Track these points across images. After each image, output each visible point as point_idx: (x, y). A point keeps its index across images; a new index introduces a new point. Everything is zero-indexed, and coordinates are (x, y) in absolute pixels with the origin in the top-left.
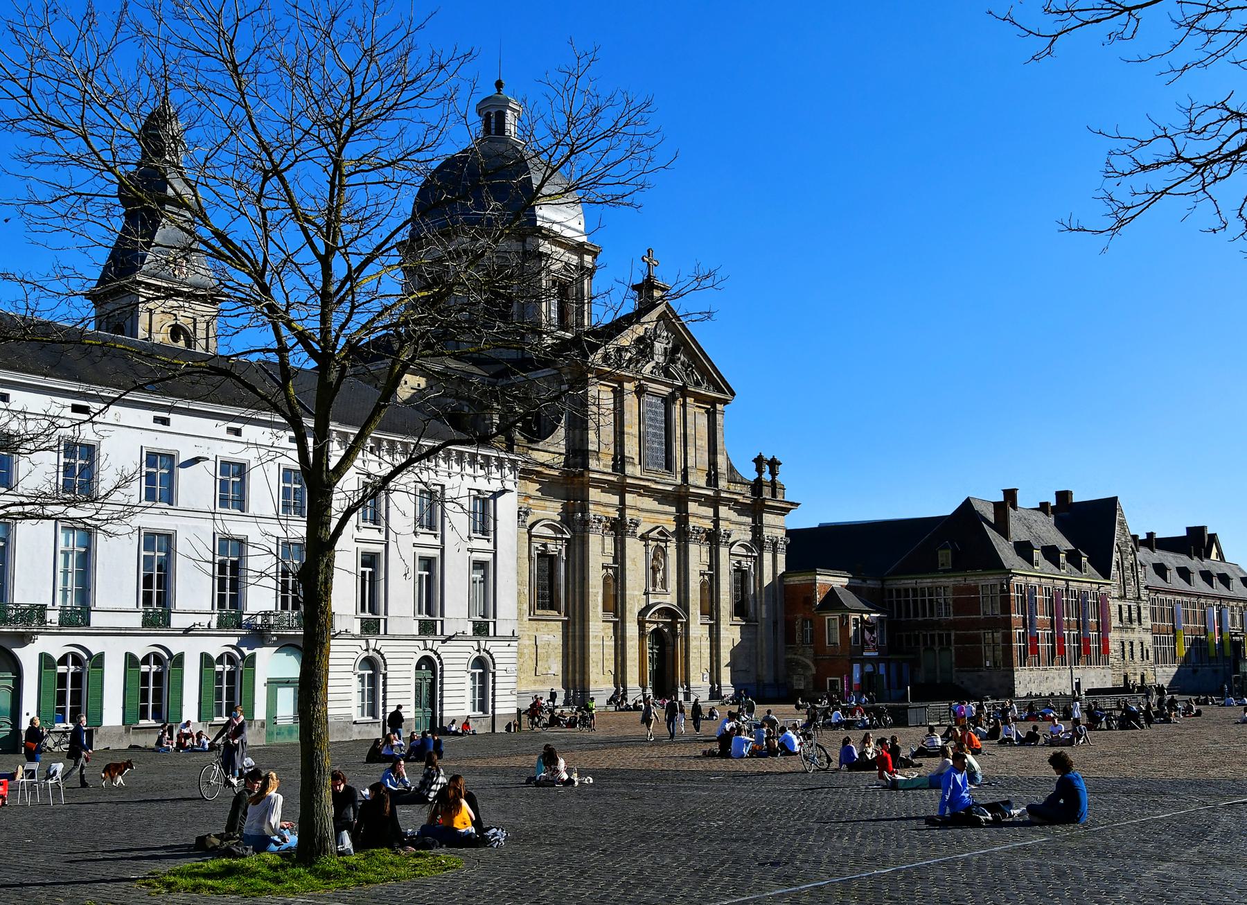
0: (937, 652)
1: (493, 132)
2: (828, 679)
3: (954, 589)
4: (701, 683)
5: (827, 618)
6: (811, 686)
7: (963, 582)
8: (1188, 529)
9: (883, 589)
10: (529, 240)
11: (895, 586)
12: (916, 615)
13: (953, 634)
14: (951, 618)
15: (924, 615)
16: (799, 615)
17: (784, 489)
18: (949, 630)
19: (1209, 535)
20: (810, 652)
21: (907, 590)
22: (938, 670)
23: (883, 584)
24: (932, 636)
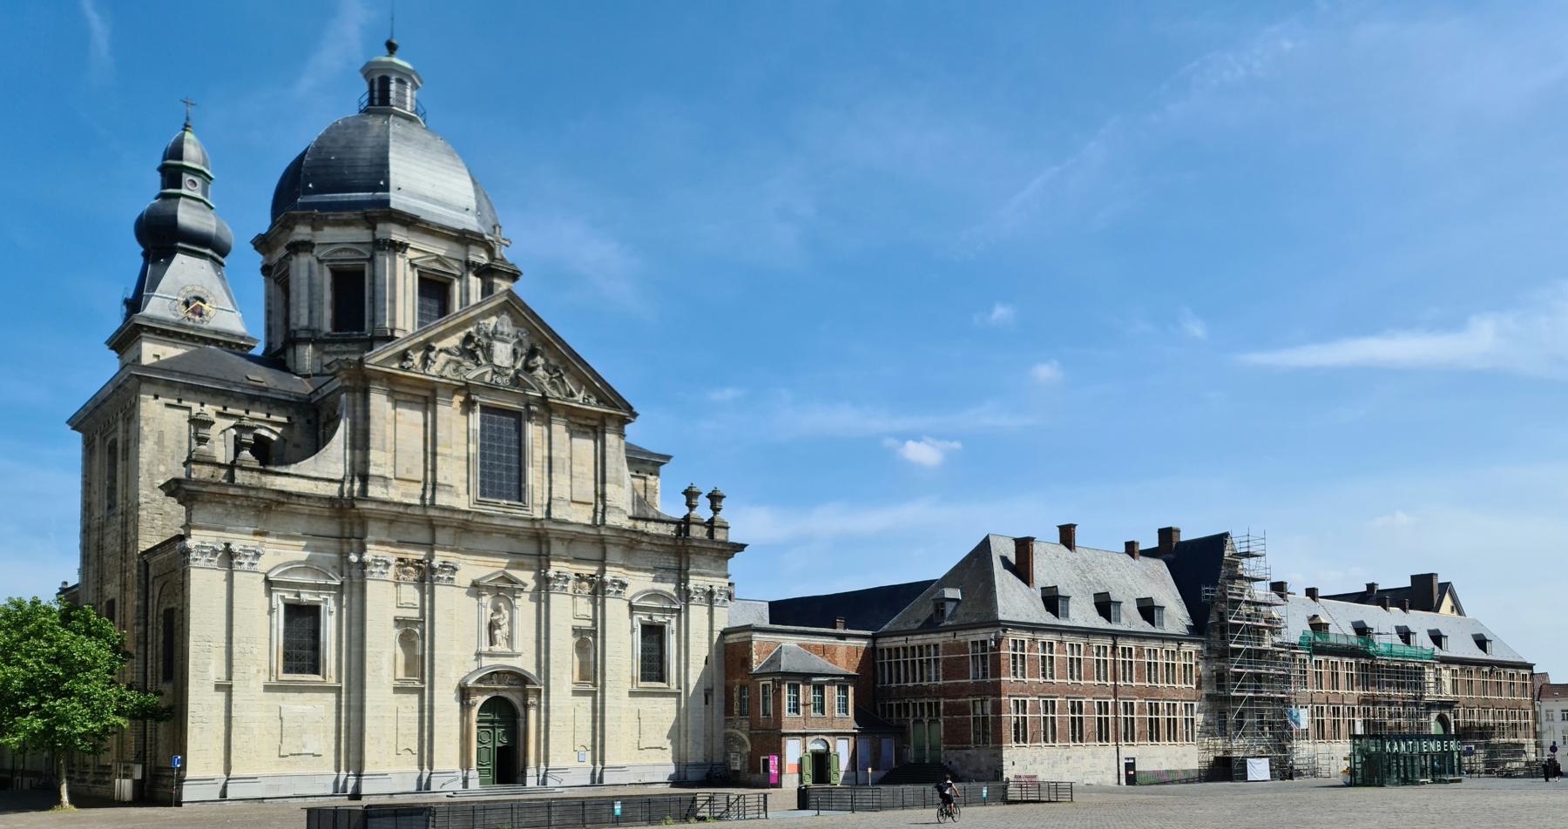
0: (926, 724)
1: (376, 102)
2: (762, 758)
3: (944, 647)
4: (572, 763)
5: (761, 683)
6: (746, 766)
7: (952, 638)
8: (1414, 578)
10: (380, 227)
11: (886, 645)
12: (906, 680)
13: (942, 703)
14: (941, 682)
15: (914, 680)
16: (738, 680)
17: (727, 528)
18: (938, 698)
19: (1440, 584)
20: (746, 724)
21: (897, 649)
22: (927, 748)
23: (874, 643)
24: (922, 705)
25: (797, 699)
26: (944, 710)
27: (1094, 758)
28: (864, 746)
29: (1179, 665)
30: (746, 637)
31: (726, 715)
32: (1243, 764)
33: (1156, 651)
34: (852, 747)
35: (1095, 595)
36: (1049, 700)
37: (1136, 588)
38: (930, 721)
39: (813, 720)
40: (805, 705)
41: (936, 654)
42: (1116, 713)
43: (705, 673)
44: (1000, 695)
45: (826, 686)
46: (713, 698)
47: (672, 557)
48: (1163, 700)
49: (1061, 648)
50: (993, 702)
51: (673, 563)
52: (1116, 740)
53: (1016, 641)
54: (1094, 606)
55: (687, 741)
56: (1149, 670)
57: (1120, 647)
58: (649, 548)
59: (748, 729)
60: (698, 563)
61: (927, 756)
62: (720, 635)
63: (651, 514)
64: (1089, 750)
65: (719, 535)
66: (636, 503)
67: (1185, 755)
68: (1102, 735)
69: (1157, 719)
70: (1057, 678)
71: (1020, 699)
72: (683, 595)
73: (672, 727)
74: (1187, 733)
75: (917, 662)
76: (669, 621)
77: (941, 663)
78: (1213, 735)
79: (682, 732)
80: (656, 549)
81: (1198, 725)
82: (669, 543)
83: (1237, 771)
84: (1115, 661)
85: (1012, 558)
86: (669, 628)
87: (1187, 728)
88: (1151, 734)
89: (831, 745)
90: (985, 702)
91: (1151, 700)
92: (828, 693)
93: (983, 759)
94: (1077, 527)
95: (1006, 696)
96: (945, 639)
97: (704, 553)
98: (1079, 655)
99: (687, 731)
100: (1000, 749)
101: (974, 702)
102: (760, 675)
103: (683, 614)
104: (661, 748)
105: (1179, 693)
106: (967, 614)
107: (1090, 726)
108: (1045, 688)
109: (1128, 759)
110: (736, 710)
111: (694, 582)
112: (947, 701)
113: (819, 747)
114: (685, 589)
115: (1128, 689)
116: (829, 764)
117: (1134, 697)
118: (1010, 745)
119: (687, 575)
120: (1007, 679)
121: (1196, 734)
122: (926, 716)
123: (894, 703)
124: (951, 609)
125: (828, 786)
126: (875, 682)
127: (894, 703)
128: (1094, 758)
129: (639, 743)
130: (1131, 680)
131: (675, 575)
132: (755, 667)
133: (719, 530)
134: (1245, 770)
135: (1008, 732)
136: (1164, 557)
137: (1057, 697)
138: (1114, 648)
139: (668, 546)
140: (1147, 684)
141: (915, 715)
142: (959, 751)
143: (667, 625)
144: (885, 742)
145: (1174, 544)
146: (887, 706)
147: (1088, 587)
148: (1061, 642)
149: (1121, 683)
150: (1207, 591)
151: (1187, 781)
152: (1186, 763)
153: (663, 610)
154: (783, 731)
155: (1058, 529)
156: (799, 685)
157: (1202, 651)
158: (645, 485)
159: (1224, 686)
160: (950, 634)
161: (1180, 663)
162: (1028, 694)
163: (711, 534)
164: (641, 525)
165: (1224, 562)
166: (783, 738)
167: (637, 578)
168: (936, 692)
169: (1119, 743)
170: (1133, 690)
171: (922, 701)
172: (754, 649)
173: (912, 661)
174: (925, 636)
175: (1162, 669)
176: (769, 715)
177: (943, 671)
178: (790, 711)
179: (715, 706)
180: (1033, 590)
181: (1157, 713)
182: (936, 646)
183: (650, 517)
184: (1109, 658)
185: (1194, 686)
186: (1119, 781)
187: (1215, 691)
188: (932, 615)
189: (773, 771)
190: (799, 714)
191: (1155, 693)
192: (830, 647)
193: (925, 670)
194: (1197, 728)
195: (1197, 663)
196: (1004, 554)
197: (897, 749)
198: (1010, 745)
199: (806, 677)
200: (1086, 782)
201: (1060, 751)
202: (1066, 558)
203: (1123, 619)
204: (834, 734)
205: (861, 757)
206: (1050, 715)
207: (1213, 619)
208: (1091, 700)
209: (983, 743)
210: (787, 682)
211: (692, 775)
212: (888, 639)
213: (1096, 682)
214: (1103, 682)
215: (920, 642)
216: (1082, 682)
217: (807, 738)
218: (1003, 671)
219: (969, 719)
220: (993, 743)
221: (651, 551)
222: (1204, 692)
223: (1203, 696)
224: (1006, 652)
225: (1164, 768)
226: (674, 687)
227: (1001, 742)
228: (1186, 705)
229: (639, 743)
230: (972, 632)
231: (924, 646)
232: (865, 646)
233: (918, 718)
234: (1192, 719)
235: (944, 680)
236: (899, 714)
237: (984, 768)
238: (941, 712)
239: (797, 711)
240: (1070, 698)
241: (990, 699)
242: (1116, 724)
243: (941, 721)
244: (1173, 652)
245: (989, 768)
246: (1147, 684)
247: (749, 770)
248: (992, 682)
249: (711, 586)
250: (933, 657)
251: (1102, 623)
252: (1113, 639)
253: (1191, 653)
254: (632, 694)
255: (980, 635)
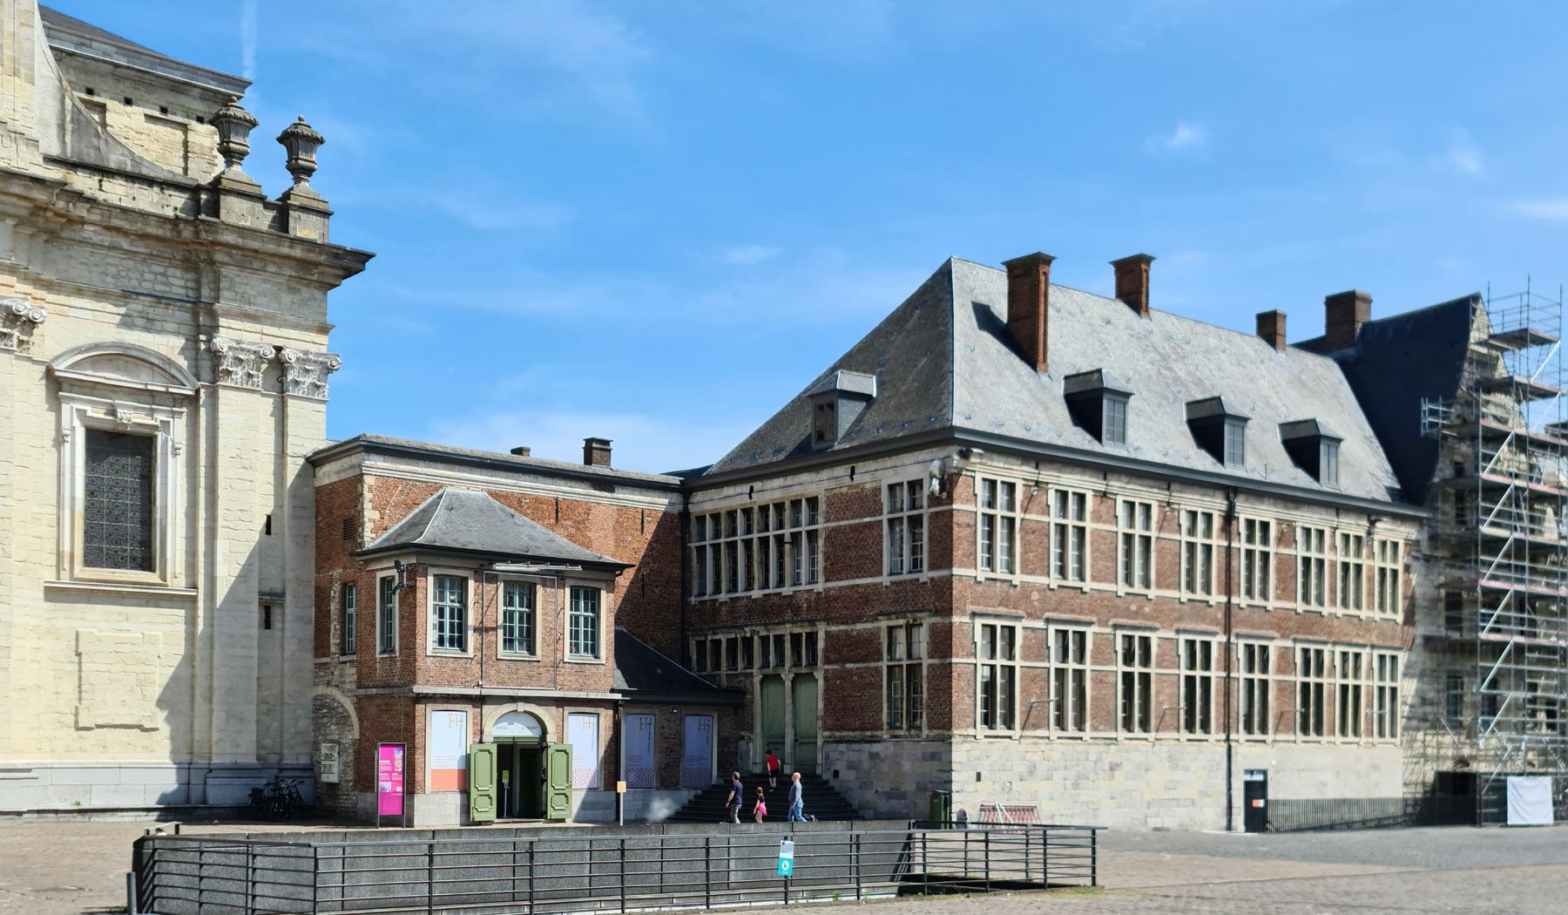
0: (788, 684)
3: (830, 503)
6: (351, 776)
7: (847, 480)
9: (685, 515)
12: (749, 587)
13: (821, 635)
14: (820, 587)
15: (766, 585)
16: (337, 573)
18: (812, 622)
20: (351, 671)
21: (732, 514)
22: (789, 740)
23: (686, 503)
24: (779, 639)
25: (461, 613)
26: (826, 650)
27: (1175, 767)
28: (640, 732)
29: (1371, 569)
30: (352, 467)
31: (317, 656)
32: (1500, 788)
33: (1321, 533)
34: (606, 734)
35: (1188, 404)
36: (1071, 629)
37: (1279, 404)
38: (797, 676)
39: (503, 665)
40: (481, 630)
41: (813, 521)
42: (1228, 668)
43: (260, 555)
44: (948, 612)
45: (540, 589)
46: (283, 614)
47: (178, 273)
48: (1335, 643)
49: (1103, 508)
50: (933, 628)
51: (178, 283)
52: (1227, 728)
53: (993, 484)
54: (1186, 428)
55: (211, 711)
56: (1306, 574)
57: (1242, 518)
58: (107, 238)
59: (354, 686)
60: (239, 284)
61: (788, 758)
62: (303, 468)
63: (113, 160)
64: (1162, 749)
65: (304, 228)
66: (69, 127)
67: (1375, 767)
68: (1195, 717)
69: (1319, 687)
70: (1094, 579)
71: (999, 623)
72: (205, 365)
73: (175, 678)
74: (1381, 718)
75: (772, 542)
76: (166, 424)
77: (821, 542)
78: (1435, 726)
79: (198, 692)
80: (125, 245)
81: (1404, 703)
82: (160, 232)
83: (1488, 804)
84: (1229, 549)
85: (1001, 310)
86: (166, 440)
87: (1381, 706)
88: (1305, 717)
89: (551, 727)
90: (915, 631)
91: (1309, 641)
92: (545, 601)
93: (907, 766)
94: (1153, 264)
95: (963, 613)
96: (832, 484)
97: (257, 265)
98: (1147, 527)
99: (211, 688)
100: (947, 740)
101: (891, 629)
102: (380, 552)
103: (203, 411)
104: (141, 728)
105: (1368, 630)
106: (884, 425)
107: (1167, 694)
108: (1061, 602)
109: (1252, 772)
110: (334, 641)
111: (230, 334)
112: (834, 628)
113: (520, 730)
114: (209, 350)
115: (1257, 615)
116: (545, 772)
117: (1271, 633)
118: (971, 731)
119: (213, 315)
120: (968, 572)
121: (1400, 723)
122: (788, 663)
123: (723, 637)
124: (853, 418)
125: (540, 824)
126: (686, 592)
127: (723, 637)
128: (1175, 767)
129: (76, 715)
130: (1264, 595)
131: (187, 317)
132: (371, 538)
133: (304, 216)
134: (1502, 803)
135: (966, 700)
136: (1337, 353)
137: (1090, 624)
138: (1229, 517)
139: (158, 239)
140: (1300, 607)
141: (765, 664)
142: (855, 746)
143: (160, 435)
144: (692, 724)
145: (1359, 326)
146: (708, 645)
147: (1175, 389)
148: (1105, 494)
149: (1240, 600)
150: (1433, 413)
151: (1380, 824)
152: (1377, 784)
153: (150, 396)
154: (417, 689)
155: (1112, 269)
156: (464, 580)
157: (1417, 542)
158: (186, 143)
159: (1460, 620)
160: (842, 471)
161: (1371, 563)
162: (1021, 613)
163: (282, 222)
164: (83, 182)
165: (1469, 353)
166: (419, 707)
167: (73, 312)
168: (809, 608)
169: (1233, 736)
170: (1267, 618)
171: (780, 630)
172: (367, 495)
173: (760, 539)
174: (790, 480)
175: (1333, 576)
176: (393, 651)
177: (827, 558)
178: (441, 641)
179: (288, 633)
180: (1044, 378)
181: (1319, 672)
182: (813, 502)
183: (113, 165)
184: (1217, 541)
185: (1400, 618)
186: (1230, 821)
187: (1443, 632)
188: (810, 435)
189: (388, 784)
190: (464, 650)
191: (1316, 628)
192: (571, 505)
193: (787, 559)
194: (1403, 710)
195: (1407, 568)
196: (983, 300)
197: (722, 742)
198: (971, 731)
199: (482, 561)
200: (1154, 822)
201: (1095, 750)
202: (1128, 327)
203: (1250, 459)
204: (560, 702)
205: (628, 759)
206: (1072, 665)
207: (1443, 471)
208: (1172, 635)
209: (909, 729)
210: (432, 571)
211: (220, 793)
212: (713, 493)
213: (1185, 595)
214: (1200, 595)
215: (777, 496)
216: (1153, 593)
217: (486, 708)
218: (957, 554)
219: (878, 671)
220: (931, 727)
221: (112, 248)
222: (1420, 630)
223: (1419, 641)
224: (969, 505)
225: (1332, 793)
226: (177, 582)
227: (948, 725)
228: (1382, 658)
229: (76, 715)
230: (889, 462)
231: (787, 505)
232: (663, 508)
233: (770, 671)
234: (1394, 690)
235: (827, 580)
236: (733, 662)
237: (909, 787)
238: (820, 654)
239: (460, 643)
240: (1122, 627)
241: (928, 621)
242: (1227, 694)
243: (819, 675)
244: (1358, 539)
245: (921, 788)
246: (1300, 607)
247: (356, 782)
248: (932, 579)
249: (279, 349)
250: (804, 528)
251: (1202, 461)
252: (1228, 498)
253: (1395, 545)
254: (54, 594)
255: (909, 467)
